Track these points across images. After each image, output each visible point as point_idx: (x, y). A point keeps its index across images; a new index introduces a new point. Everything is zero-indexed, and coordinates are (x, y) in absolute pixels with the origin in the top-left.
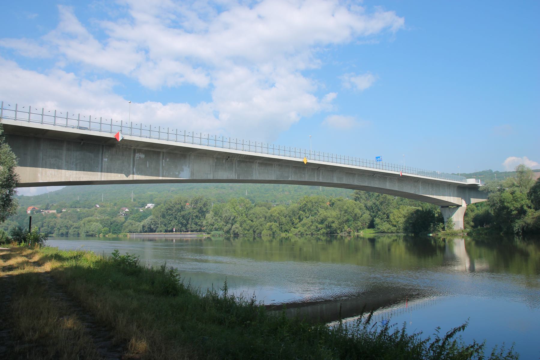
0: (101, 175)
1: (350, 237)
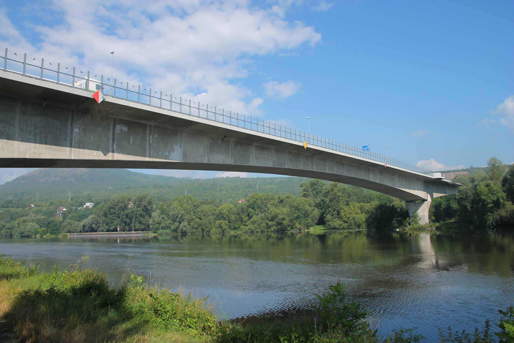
0: (71, 151)
1: (301, 234)
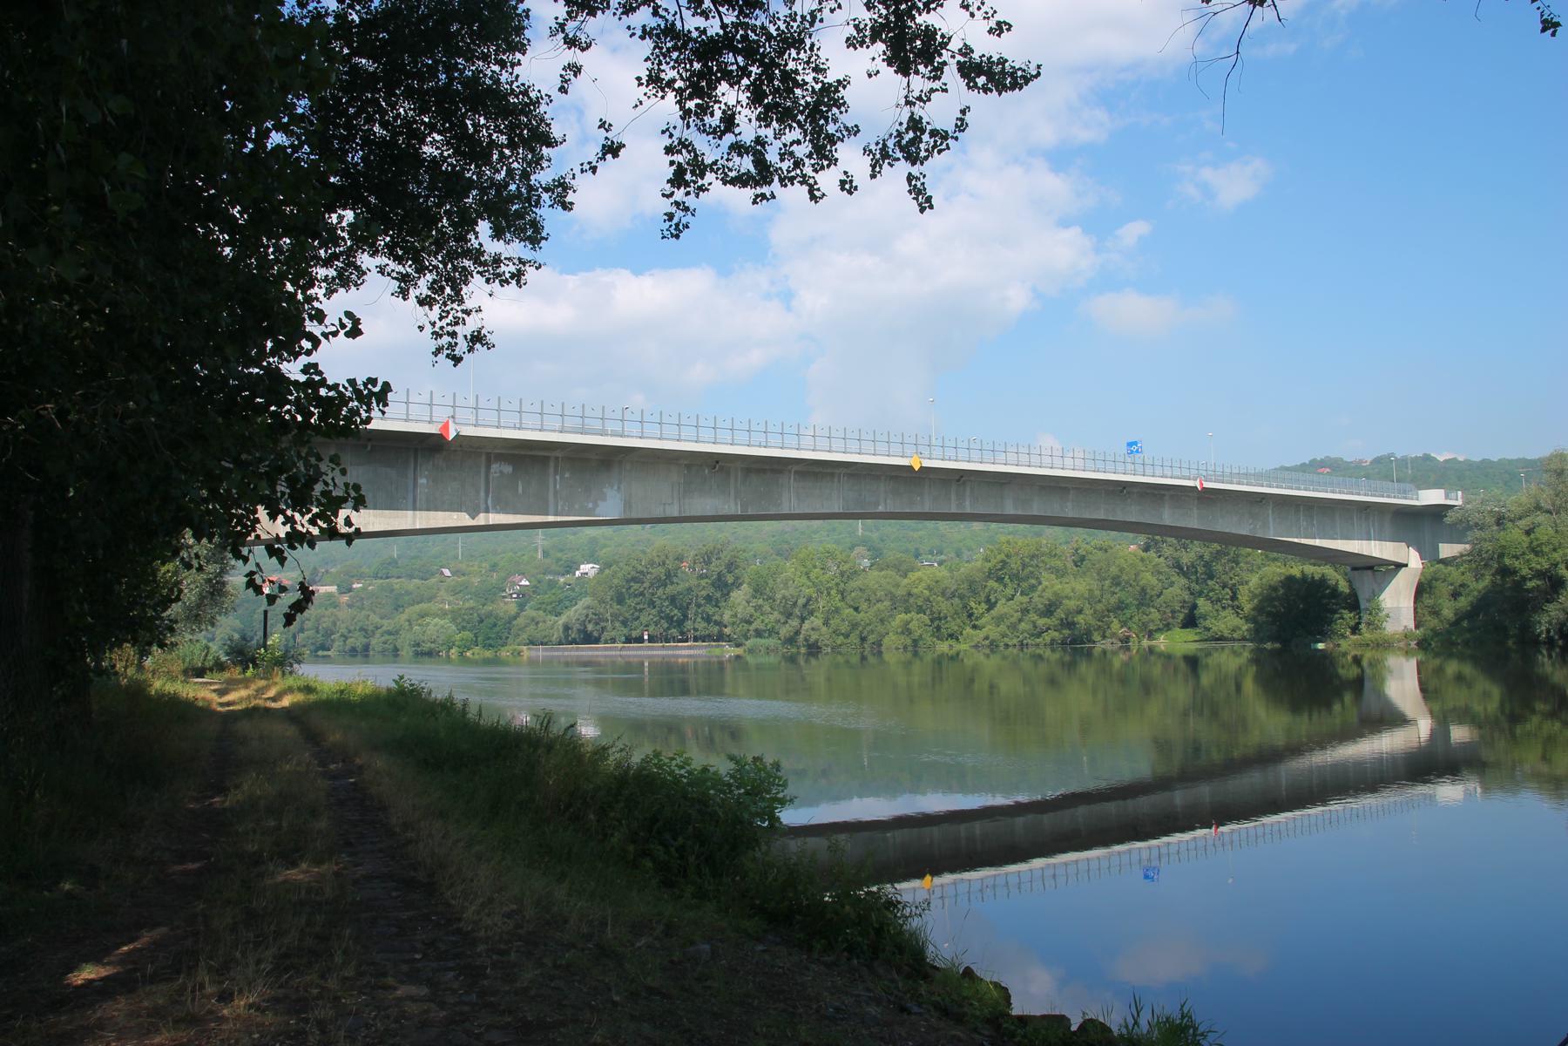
0: (414, 516)
1: (1127, 653)
